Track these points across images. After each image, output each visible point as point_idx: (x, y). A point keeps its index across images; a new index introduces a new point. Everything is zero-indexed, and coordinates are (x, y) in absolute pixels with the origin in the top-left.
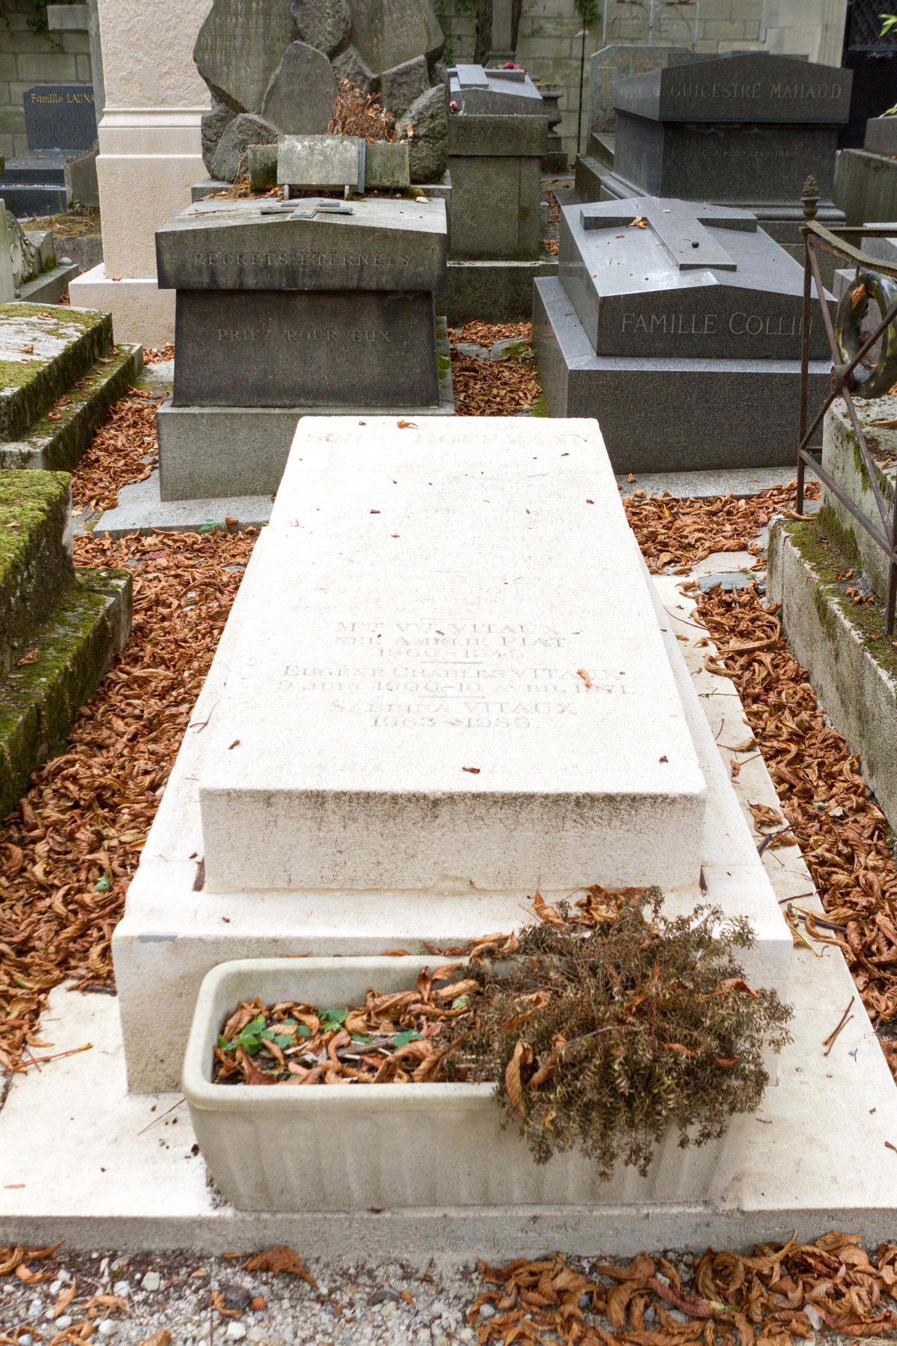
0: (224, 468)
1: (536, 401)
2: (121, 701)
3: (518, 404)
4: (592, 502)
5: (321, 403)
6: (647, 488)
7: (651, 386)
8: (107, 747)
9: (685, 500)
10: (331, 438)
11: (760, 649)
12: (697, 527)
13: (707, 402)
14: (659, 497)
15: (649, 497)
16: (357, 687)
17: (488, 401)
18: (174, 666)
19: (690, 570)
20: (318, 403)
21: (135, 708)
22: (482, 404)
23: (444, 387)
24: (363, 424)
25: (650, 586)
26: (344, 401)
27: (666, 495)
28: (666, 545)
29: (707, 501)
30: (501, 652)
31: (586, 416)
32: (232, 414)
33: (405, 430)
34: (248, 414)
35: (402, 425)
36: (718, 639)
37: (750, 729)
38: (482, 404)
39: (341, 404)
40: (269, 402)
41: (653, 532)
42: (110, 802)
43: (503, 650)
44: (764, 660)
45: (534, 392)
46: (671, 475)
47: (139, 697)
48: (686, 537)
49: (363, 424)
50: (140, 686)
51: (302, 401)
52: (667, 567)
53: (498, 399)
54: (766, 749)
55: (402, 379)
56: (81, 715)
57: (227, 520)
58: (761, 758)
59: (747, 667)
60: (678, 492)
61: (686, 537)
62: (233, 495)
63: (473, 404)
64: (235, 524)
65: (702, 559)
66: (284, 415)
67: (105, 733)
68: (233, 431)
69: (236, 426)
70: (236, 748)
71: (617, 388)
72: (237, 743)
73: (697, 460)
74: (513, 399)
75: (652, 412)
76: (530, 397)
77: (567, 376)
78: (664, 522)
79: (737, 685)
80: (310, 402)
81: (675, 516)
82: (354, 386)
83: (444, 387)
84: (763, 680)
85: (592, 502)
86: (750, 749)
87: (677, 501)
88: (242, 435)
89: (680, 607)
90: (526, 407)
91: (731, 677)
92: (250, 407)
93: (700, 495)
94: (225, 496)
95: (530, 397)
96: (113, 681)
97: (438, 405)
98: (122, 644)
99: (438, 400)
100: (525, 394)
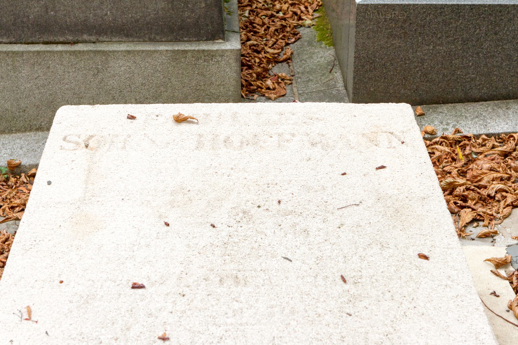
0: (7, 105)
1: (316, 15)
3: (300, 19)
4: (426, 258)
5: (105, 38)
6: (436, 123)
7: (440, 19)
9: (477, 137)
10: (91, 144)
12: (495, 175)
13: (496, 34)
14: (450, 133)
15: (439, 134)
17: (272, 16)
19: (496, 233)
20: (101, 39)
22: (266, 20)
23: (229, 13)
24: (132, 118)
26: (127, 36)
27: (458, 131)
28: (465, 199)
29: (502, 138)
31: (398, 101)
32: (13, 53)
33: (184, 126)
34: (29, 52)
35: (180, 120)
38: (266, 20)
39: (125, 39)
40: (51, 39)
41: (450, 184)
45: (314, 6)
46: (459, 106)
48: (485, 187)
49: (132, 118)
51: (85, 37)
52: (470, 228)
53: (281, 14)
55: (186, 14)
57: (9, 163)
60: (470, 129)
61: (485, 187)
62: (18, 131)
63: (258, 20)
64: (19, 166)
65: (506, 217)
66: (66, 52)
68: (15, 69)
69: (17, 64)
71: (405, 21)
73: (485, 90)
74: (295, 13)
75: (441, 45)
76: (311, 11)
77: (354, 11)
78: (459, 165)
80: (93, 38)
81: (470, 161)
82: (137, 21)
83: (229, 13)
85: (426, 258)
87: (469, 138)
88: (25, 71)
89: (494, 294)
90: (308, 22)
92: (32, 43)
93: (491, 131)
94: (10, 132)
95: (311, 11)
97: (223, 39)
99: (223, 32)
100: (306, 8)
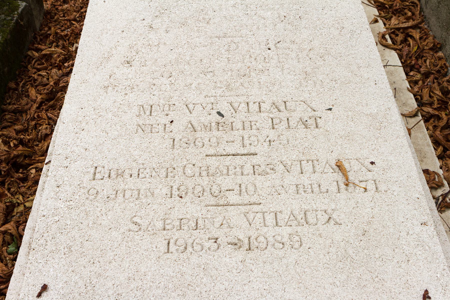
2: (35, 73)
8: (26, 112)
11: (411, 27)
16: (153, 194)
18: (68, 40)
21: (43, 77)
25: (382, 56)
30: (271, 138)
36: (383, 17)
37: (412, 96)
42: (24, 163)
43: (272, 135)
44: (414, 36)
47: (46, 69)
50: (47, 61)
54: (424, 113)
56: (10, 89)
58: (422, 122)
59: (405, 41)
67: (24, 101)
70: (44, 294)
72: (45, 288)
79: (401, 57)
84: (415, 52)
86: (415, 115)
91: (395, 50)
96: (31, 57)
98: (38, 25)
